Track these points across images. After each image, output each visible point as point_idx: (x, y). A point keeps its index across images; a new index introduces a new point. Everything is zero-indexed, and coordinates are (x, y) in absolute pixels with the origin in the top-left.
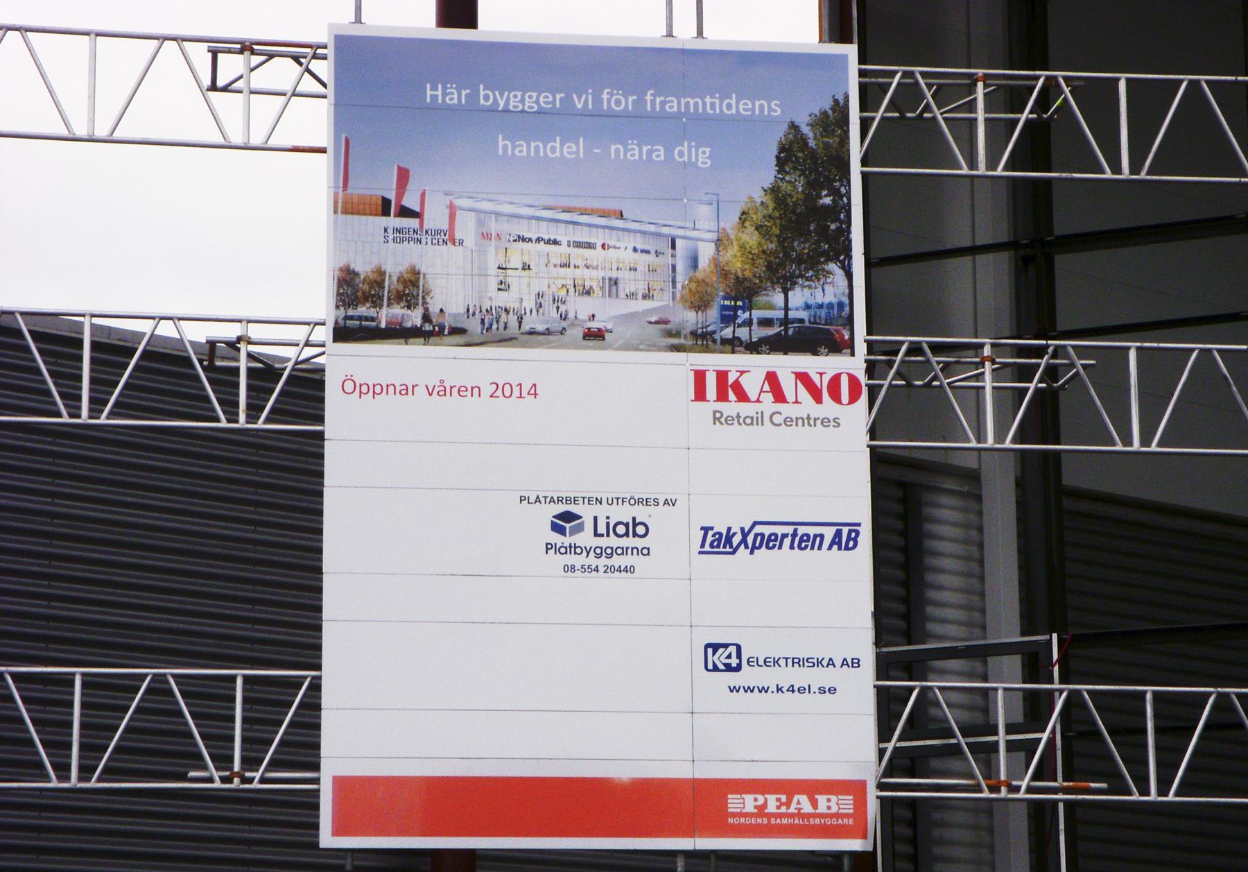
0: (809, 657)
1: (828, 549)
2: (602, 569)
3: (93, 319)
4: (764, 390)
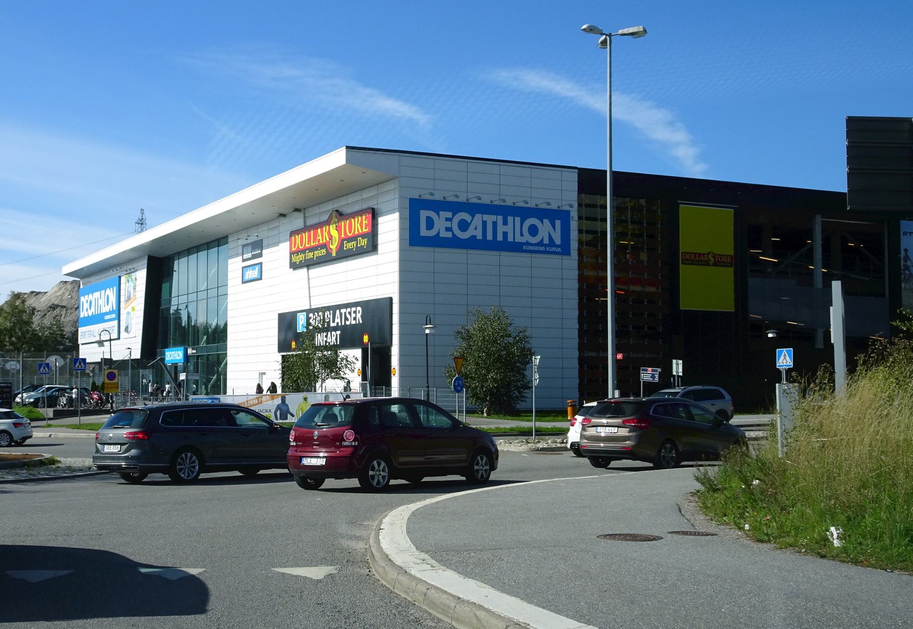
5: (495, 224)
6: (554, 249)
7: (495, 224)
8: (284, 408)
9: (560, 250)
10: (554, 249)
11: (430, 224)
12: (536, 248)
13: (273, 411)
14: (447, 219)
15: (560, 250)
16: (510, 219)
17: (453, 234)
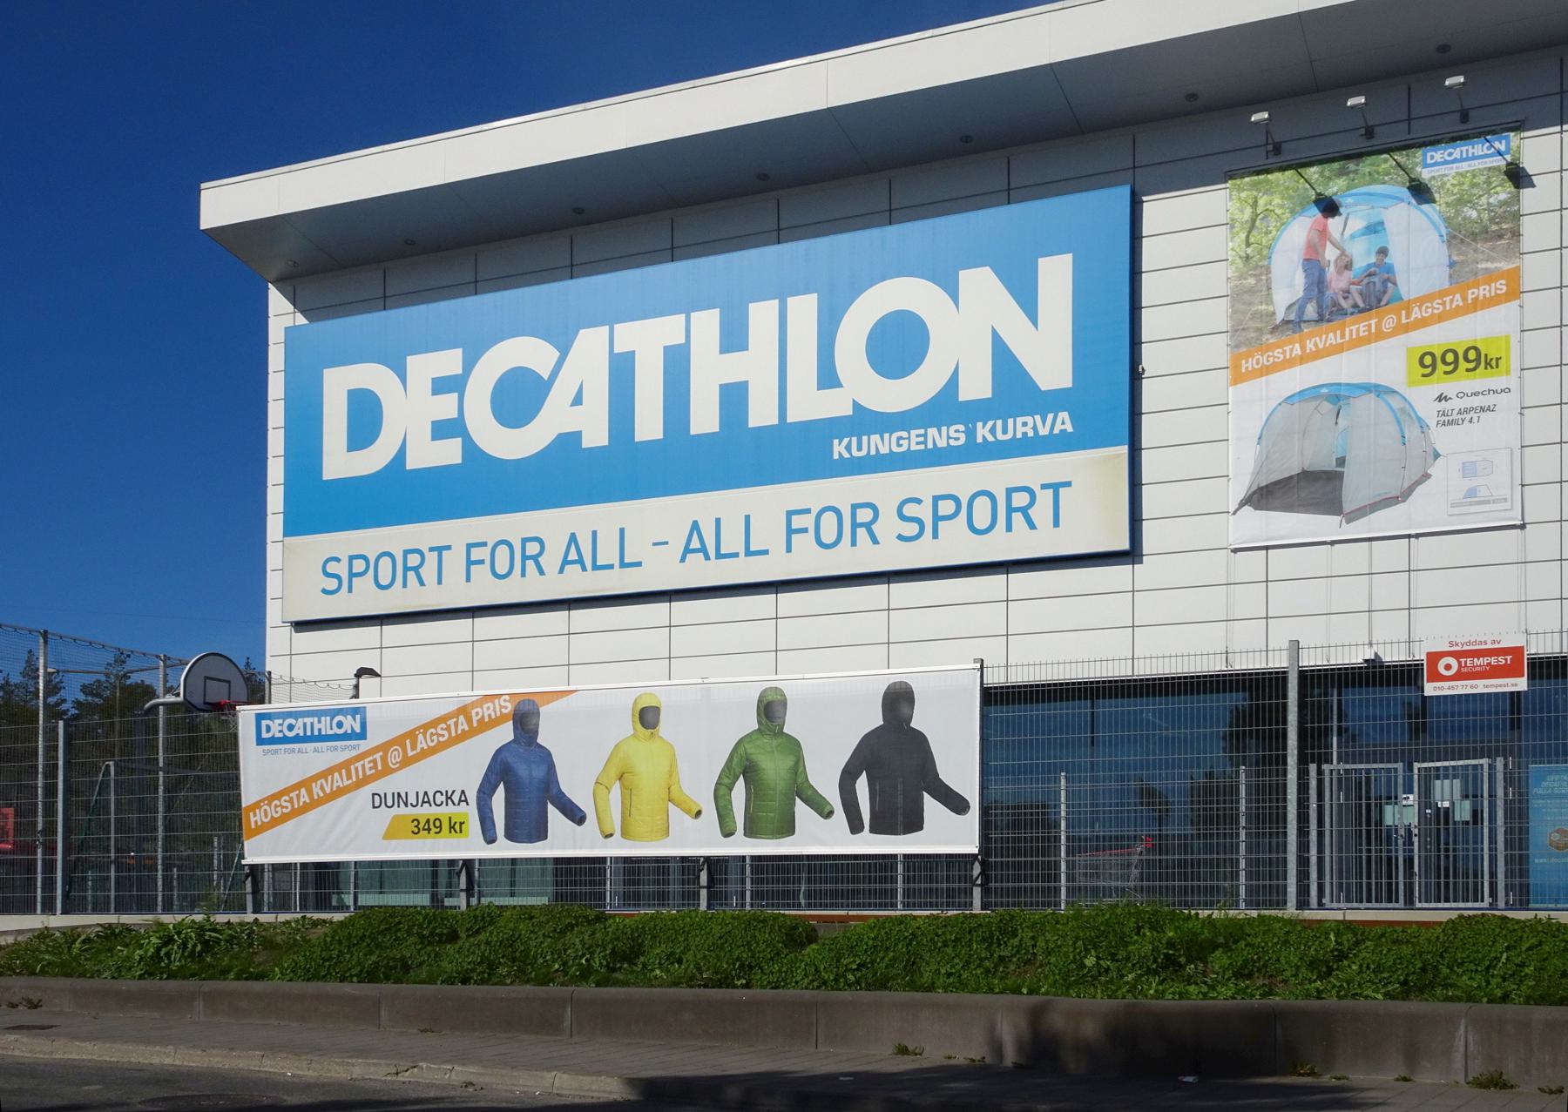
0: (232, 685)
1: (680, 562)
2: (324, 749)
3: (1445, 798)
4: (692, 547)
5: (312, 724)
6: (1022, 426)
7: (312, 724)
8: (773, 768)
9: (1064, 422)
10: (1022, 426)
11: (268, 729)
12: (912, 441)
13: (472, 797)
14: (441, 386)
15: (1064, 422)
16: (323, 718)
17: (470, 448)
